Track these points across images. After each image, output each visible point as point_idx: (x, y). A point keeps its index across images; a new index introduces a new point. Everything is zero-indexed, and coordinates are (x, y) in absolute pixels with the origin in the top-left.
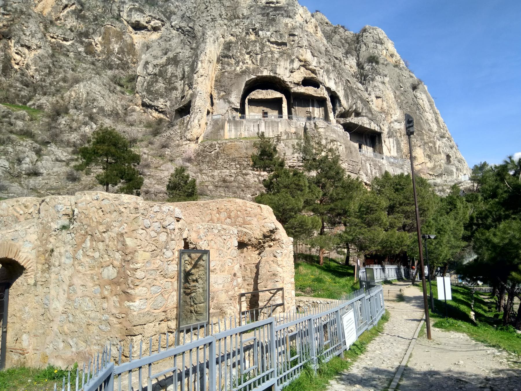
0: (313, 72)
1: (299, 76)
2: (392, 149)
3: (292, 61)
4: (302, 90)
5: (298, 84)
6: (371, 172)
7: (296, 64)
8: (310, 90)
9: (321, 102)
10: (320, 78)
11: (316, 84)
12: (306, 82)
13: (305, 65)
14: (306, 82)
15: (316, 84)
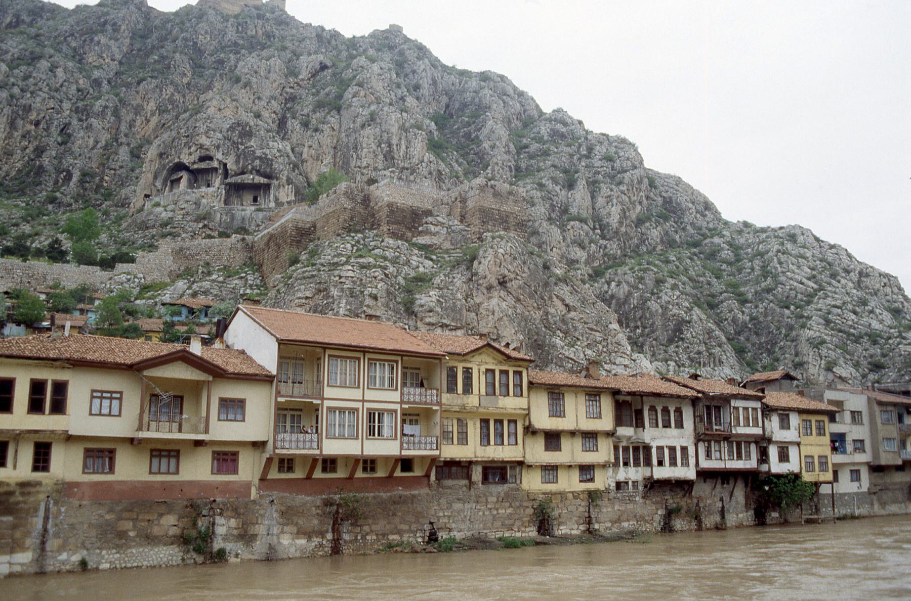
0: (207, 149)
1: (195, 157)
3: (190, 148)
4: (196, 166)
5: (194, 163)
7: (193, 149)
8: (203, 165)
9: (216, 169)
10: (212, 154)
11: (210, 158)
12: (202, 159)
13: (201, 147)
14: (202, 159)
15: (210, 158)
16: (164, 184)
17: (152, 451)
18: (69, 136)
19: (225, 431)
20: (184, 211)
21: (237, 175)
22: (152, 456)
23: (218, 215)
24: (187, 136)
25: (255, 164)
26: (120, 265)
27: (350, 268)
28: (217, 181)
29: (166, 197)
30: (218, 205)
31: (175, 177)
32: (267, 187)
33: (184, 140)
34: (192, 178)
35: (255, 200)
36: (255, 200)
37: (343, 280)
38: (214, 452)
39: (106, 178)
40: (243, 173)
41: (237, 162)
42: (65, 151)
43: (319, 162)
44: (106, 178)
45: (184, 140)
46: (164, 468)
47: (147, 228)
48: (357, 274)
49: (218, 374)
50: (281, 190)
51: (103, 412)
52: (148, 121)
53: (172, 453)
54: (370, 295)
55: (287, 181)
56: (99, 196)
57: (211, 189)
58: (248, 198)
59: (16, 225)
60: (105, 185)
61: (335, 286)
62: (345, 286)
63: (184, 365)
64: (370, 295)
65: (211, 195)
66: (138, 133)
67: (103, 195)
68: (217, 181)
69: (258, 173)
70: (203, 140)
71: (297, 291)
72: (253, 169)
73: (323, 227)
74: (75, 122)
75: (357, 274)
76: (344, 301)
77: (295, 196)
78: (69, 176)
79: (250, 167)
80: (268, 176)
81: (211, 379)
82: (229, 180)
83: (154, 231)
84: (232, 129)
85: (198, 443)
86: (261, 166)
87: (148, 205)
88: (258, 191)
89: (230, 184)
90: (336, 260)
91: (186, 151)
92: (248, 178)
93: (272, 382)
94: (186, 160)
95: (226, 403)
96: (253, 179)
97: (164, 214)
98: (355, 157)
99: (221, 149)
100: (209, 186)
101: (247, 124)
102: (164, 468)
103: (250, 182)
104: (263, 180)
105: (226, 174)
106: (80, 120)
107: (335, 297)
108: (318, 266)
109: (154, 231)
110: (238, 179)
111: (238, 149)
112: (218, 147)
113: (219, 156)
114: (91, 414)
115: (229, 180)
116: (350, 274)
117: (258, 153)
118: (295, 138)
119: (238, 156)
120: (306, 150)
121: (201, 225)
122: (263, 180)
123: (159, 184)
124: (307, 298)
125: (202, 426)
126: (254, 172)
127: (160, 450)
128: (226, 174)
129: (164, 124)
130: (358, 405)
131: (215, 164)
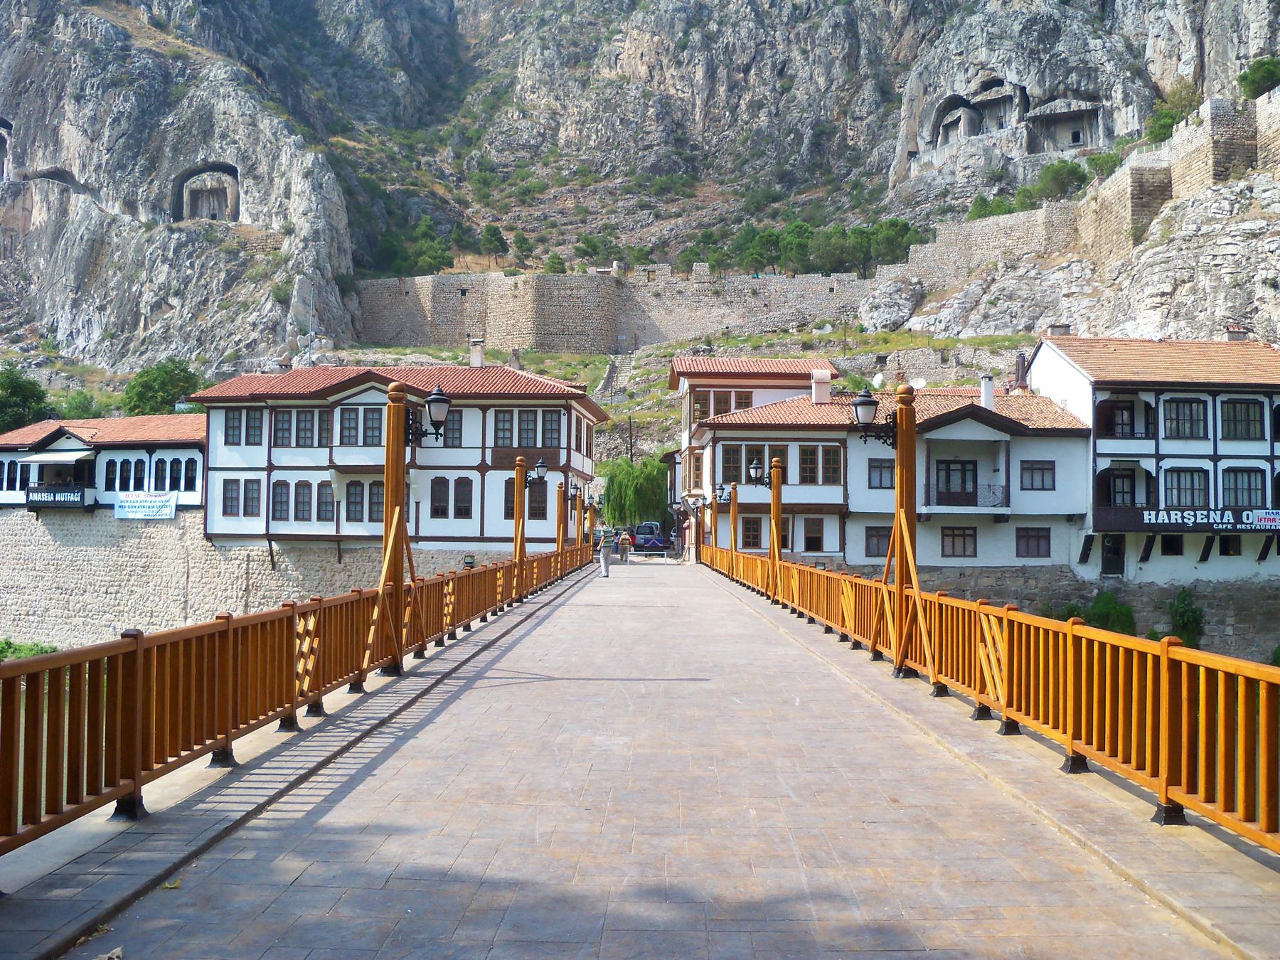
0: (993, 69)
1: (974, 86)
2: (1130, 120)
3: (967, 70)
4: (978, 99)
5: (975, 94)
6: (1025, 176)
7: (972, 71)
10: (1000, 75)
11: (1000, 83)
12: (987, 86)
13: (983, 66)
14: (987, 86)
15: (1000, 83)
16: (935, 133)
17: (943, 529)
18: (792, 78)
19: (1029, 503)
20: (968, 172)
21: (1042, 102)
22: (943, 536)
23: (1021, 170)
24: (961, 53)
25: (1069, 81)
26: (885, 267)
27: (1229, 240)
28: (1013, 117)
29: (939, 157)
30: (1017, 154)
31: (949, 119)
32: (1093, 113)
33: (957, 60)
34: (974, 115)
35: (1076, 138)
36: (1076, 138)
37: (1218, 261)
38: (1018, 530)
39: (850, 133)
40: (1052, 98)
41: (1041, 82)
42: (788, 101)
43: (1175, 58)
44: (850, 133)
45: (957, 60)
46: (959, 550)
47: (918, 203)
48: (1239, 249)
49: (1016, 430)
50: (1115, 116)
51: (959, 467)
52: (901, 35)
53: (968, 532)
54: (1264, 282)
55: (1124, 100)
56: (842, 163)
57: (1005, 133)
58: (1065, 136)
59: (739, 221)
60: (851, 143)
61: (1207, 272)
62: (1224, 271)
63: (975, 423)
64: (1264, 282)
65: (1008, 136)
66: (888, 56)
67: (849, 160)
68: (1013, 117)
69: (1078, 94)
70: (983, 55)
71: (1147, 284)
72: (1067, 88)
73: (1183, 176)
74: (796, 55)
75: (1239, 249)
76: (1223, 295)
77: (1140, 123)
78: (799, 137)
79: (1061, 87)
80: (1093, 97)
81: (1007, 437)
82: (1031, 113)
83: (927, 207)
84: (1026, 29)
85: (1000, 519)
86: (1079, 83)
87: (915, 170)
88: (1078, 124)
89: (1034, 120)
90: (1205, 229)
91: (961, 76)
92: (1059, 106)
93: (1087, 437)
94: (962, 90)
95: (1029, 467)
96: (1069, 105)
97: (939, 180)
98: (1236, 41)
99: (1014, 65)
100: (1001, 126)
101: (1050, 17)
102: (959, 550)
103: (1065, 110)
104: (1085, 105)
105: (1026, 102)
106: (804, 52)
107: (1208, 290)
108: (1179, 242)
109: (927, 207)
110: (1046, 109)
111: (1041, 61)
112: (1009, 62)
113: (1012, 77)
114: (870, 487)
115: (1031, 113)
116: (1231, 249)
117: (1073, 62)
118: (1128, 25)
119: (1042, 73)
120: (1150, 42)
121: (995, 190)
122: (1085, 105)
123: (926, 134)
124: (1163, 294)
125: (1000, 495)
126: (1069, 93)
127: (953, 529)
128: (1026, 102)
129: (924, 36)
130: (1208, 465)
131: (1007, 90)
